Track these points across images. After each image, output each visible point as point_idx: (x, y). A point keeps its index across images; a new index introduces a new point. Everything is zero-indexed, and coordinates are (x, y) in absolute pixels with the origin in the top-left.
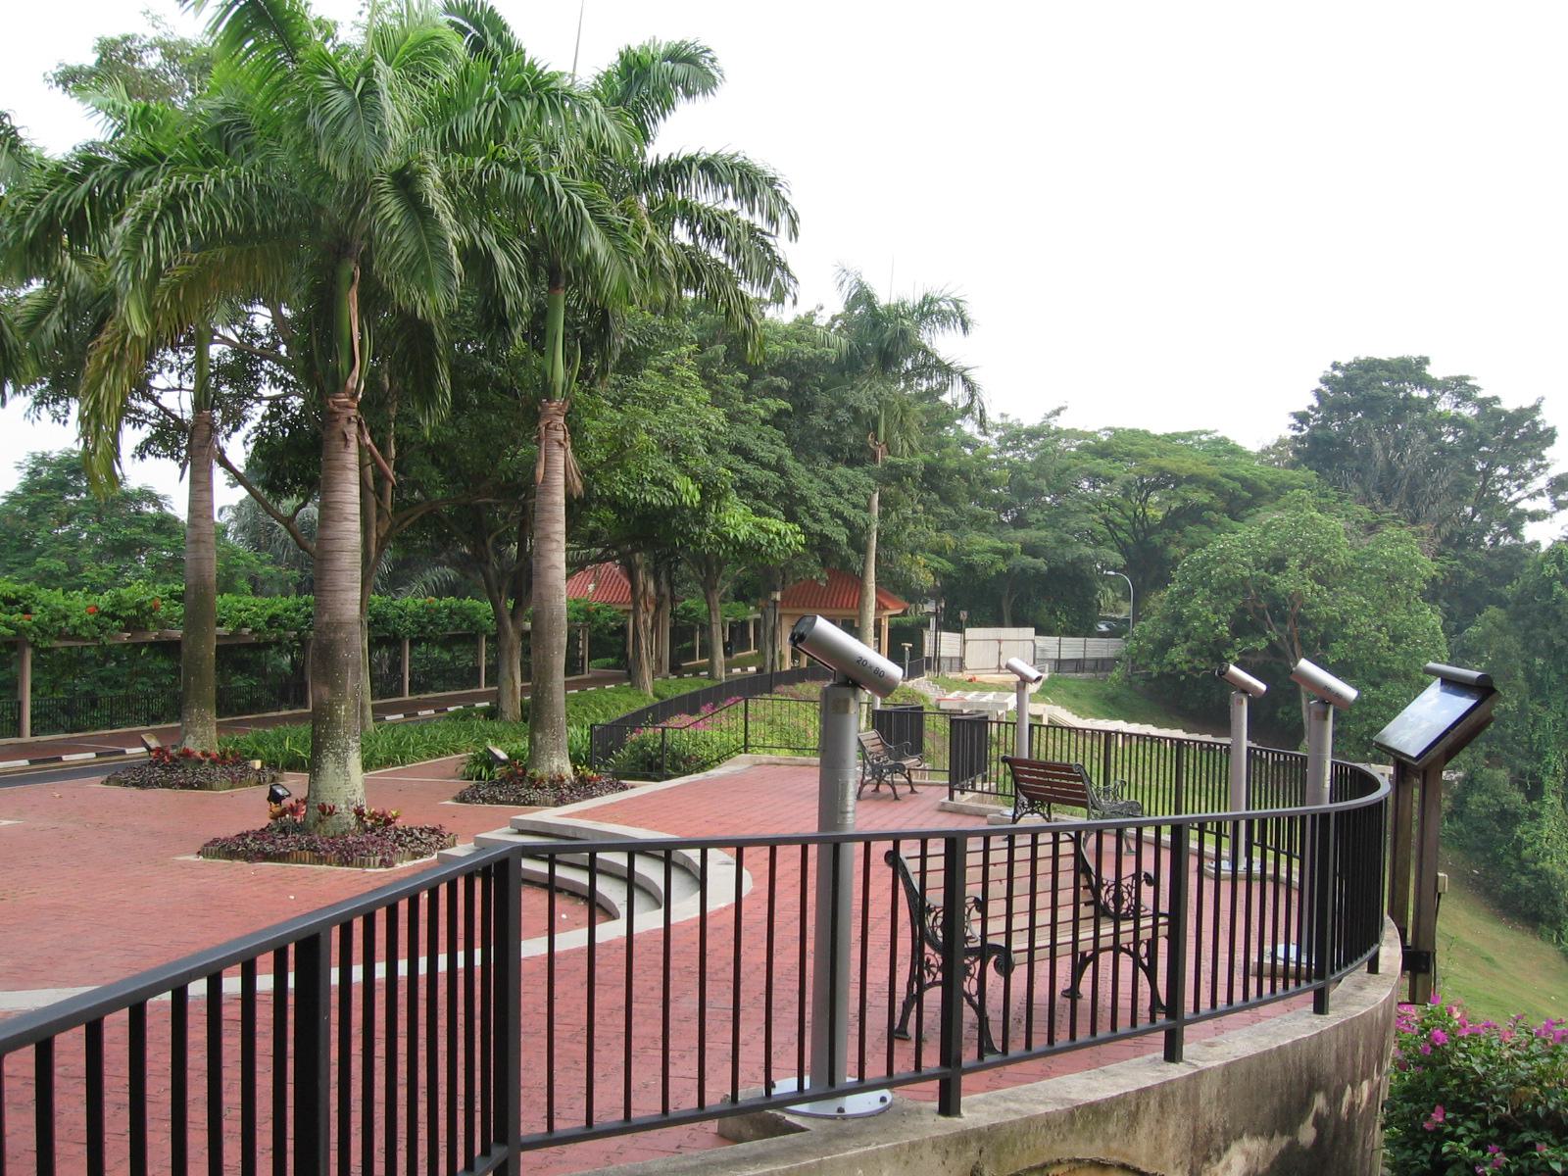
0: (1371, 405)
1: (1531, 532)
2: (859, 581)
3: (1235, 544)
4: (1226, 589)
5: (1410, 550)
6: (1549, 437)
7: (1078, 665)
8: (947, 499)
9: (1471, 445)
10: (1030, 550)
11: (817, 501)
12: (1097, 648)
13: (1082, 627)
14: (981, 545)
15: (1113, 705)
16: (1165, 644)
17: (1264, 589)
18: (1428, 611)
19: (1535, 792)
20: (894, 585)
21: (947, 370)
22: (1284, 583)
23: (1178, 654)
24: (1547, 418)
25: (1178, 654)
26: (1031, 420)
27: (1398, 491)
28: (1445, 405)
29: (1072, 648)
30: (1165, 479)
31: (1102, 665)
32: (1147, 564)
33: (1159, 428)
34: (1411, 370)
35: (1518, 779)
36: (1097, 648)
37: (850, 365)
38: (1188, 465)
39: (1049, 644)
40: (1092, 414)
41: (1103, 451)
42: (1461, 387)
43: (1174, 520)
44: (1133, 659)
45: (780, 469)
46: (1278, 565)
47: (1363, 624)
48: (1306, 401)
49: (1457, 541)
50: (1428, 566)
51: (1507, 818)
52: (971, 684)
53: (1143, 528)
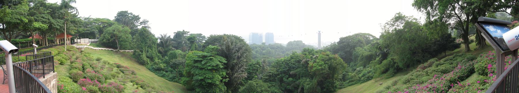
0: (122, 15)
1: (139, 27)
2: (64, 33)
3: (110, 29)
4: (109, 34)
5: (127, 29)
6: (140, 18)
7: (94, 42)
8: (77, 24)
9: (132, 19)
10: (88, 30)
11: (55, 23)
12: (96, 40)
13: (94, 38)
14: (81, 29)
15: (98, 46)
16: (103, 39)
17: (113, 33)
18: (8, 10)
19: (142, 52)
20: (69, 34)
21: (74, 8)
22: (115, 33)
23: (105, 40)
24: (140, 16)
25: (105, 40)
26: (87, 17)
27: (126, 23)
28: (130, 15)
29: (93, 40)
30: (103, 23)
31: (96, 42)
32: (101, 31)
33: (101, 18)
34: (126, 12)
35: (140, 51)
36: (96, 40)
37: (61, 7)
38: (105, 21)
39: (90, 40)
40: (94, 16)
41: (96, 20)
42: (131, 14)
43: (103, 27)
44: (100, 41)
45: (49, 19)
46: (114, 31)
47: (123, 36)
48: (116, 15)
49: (131, 28)
50: (130, 30)
51: (140, 55)
52: (82, 45)
53: (100, 28)
